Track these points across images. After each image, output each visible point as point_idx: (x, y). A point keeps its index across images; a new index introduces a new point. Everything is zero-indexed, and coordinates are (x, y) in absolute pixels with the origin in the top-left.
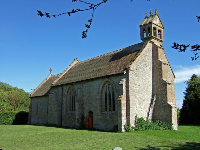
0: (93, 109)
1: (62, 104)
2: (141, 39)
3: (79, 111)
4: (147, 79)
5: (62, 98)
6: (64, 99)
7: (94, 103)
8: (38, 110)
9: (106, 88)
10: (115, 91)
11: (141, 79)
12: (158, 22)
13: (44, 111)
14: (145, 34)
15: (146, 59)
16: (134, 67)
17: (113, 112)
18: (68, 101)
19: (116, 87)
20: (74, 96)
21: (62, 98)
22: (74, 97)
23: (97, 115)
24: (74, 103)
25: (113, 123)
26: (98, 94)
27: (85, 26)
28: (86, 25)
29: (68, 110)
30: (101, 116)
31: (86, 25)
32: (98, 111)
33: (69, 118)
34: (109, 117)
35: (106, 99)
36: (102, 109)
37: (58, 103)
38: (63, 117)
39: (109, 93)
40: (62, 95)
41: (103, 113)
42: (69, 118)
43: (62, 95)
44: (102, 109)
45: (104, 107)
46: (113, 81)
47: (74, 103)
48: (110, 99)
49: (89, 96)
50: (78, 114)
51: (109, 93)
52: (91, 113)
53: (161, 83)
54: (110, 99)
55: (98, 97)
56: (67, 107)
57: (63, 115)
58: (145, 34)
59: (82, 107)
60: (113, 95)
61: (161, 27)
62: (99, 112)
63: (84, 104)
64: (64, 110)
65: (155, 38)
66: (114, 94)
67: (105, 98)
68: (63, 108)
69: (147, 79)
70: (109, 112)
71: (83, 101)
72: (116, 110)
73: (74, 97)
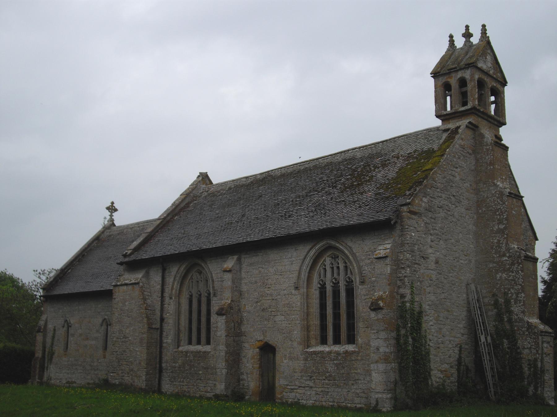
0: (274, 339)
1: (162, 320)
2: (438, 116)
3: (227, 346)
4: (458, 241)
5: (162, 301)
6: (171, 307)
7: (279, 318)
8: (71, 339)
9: (325, 269)
10: (357, 280)
11: (441, 242)
12: (490, 65)
13: (93, 342)
14: (448, 98)
15: (458, 178)
16: (423, 204)
17: (350, 348)
18: (182, 329)
19: (360, 268)
20: (204, 294)
21: (162, 301)
22: (204, 300)
23: (291, 358)
24: (203, 319)
25: (351, 382)
26: (297, 288)
27: (109, 204)
28: (113, 203)
29: (184, 337)
30: (306, 359)
31: (113, 203)
32: (295, 344)
33: (187, 367)
34: (337, 365)
35: (323, 306)
36: (308, 337)
37: (147, 317)
38: (164, 365)
39: (336, 286)
40: (163, 291)
41: (315, 353)
42: (187, 367)
43: (163, 291)
44: (308, 337)
45: (315, 331)
46: (350, 248)
47: (203, 319)
48: (336, 305)
49: (262, 296)
50: (223, 354)
51: (336, 286)
52: (267, 350)
53: (504, 255)
54: (336, 305)
55: (297, 300)
56: (179, 331)
57: (165, 358)
58: (448, 98)
59: (236, 333)
60: (350, 292)
61: (499, 81)
62: (298, 349)
63: (245, 322)
64: (169, 339)
65: (483, 113)
66: (353, 289)
67: (318, 301)
68: (165, 334)
69: (458, 241)
70: (336, 348)
71: (239, 310)
72: (360, 340)
73: (204, 300)
